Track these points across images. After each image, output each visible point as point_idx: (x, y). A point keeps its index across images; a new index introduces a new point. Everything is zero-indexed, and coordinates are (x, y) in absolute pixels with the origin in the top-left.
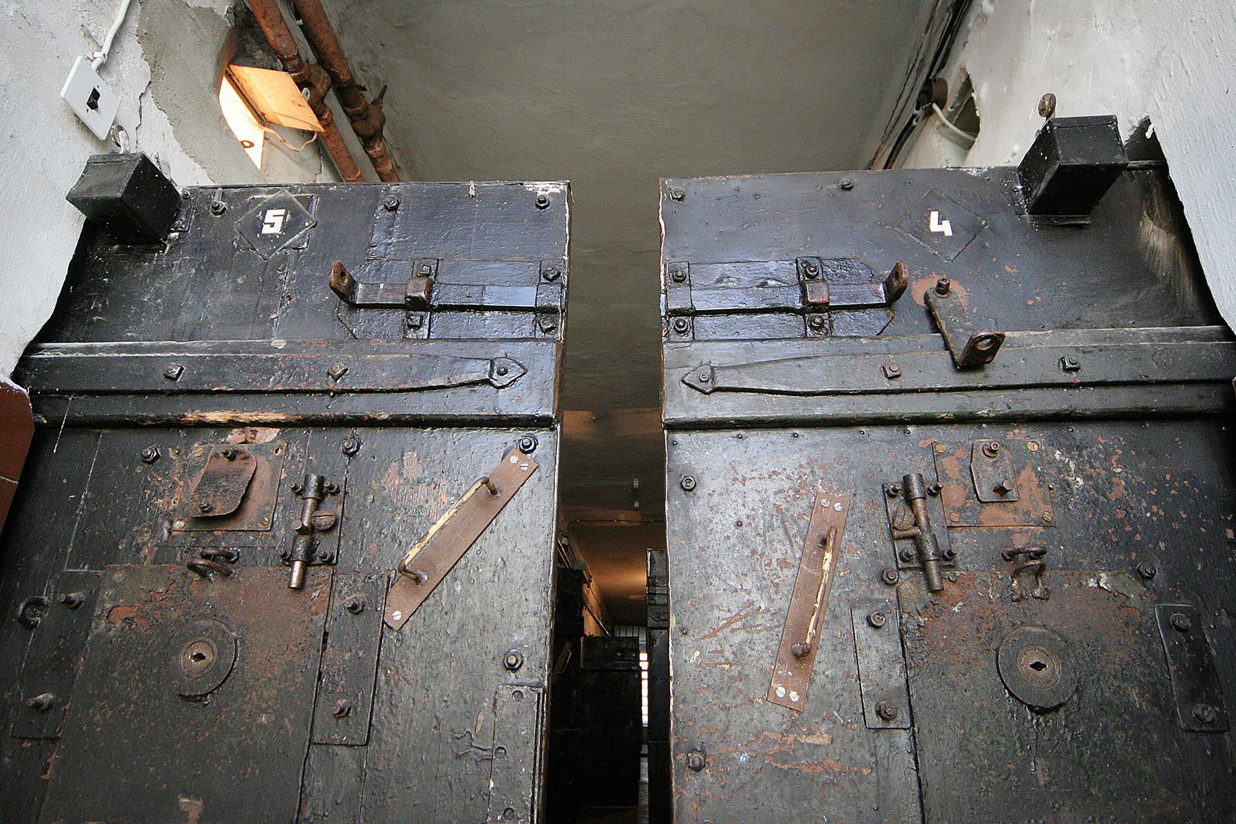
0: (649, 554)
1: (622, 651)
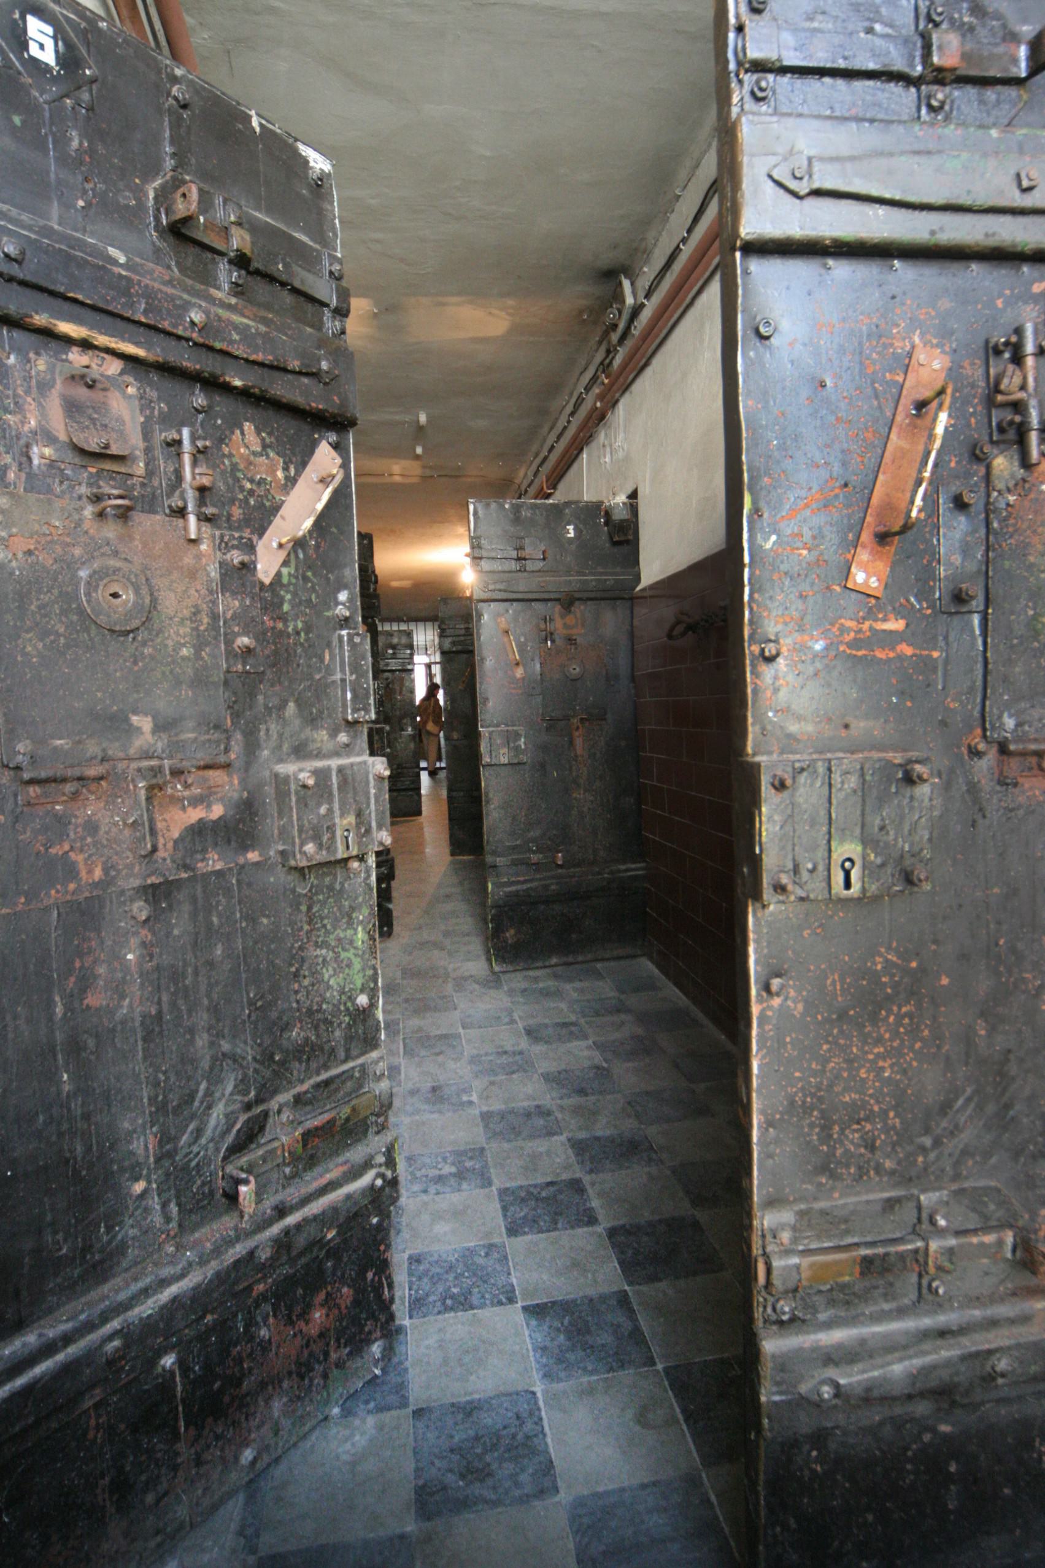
0: (471, 507)
1: (394, 647)
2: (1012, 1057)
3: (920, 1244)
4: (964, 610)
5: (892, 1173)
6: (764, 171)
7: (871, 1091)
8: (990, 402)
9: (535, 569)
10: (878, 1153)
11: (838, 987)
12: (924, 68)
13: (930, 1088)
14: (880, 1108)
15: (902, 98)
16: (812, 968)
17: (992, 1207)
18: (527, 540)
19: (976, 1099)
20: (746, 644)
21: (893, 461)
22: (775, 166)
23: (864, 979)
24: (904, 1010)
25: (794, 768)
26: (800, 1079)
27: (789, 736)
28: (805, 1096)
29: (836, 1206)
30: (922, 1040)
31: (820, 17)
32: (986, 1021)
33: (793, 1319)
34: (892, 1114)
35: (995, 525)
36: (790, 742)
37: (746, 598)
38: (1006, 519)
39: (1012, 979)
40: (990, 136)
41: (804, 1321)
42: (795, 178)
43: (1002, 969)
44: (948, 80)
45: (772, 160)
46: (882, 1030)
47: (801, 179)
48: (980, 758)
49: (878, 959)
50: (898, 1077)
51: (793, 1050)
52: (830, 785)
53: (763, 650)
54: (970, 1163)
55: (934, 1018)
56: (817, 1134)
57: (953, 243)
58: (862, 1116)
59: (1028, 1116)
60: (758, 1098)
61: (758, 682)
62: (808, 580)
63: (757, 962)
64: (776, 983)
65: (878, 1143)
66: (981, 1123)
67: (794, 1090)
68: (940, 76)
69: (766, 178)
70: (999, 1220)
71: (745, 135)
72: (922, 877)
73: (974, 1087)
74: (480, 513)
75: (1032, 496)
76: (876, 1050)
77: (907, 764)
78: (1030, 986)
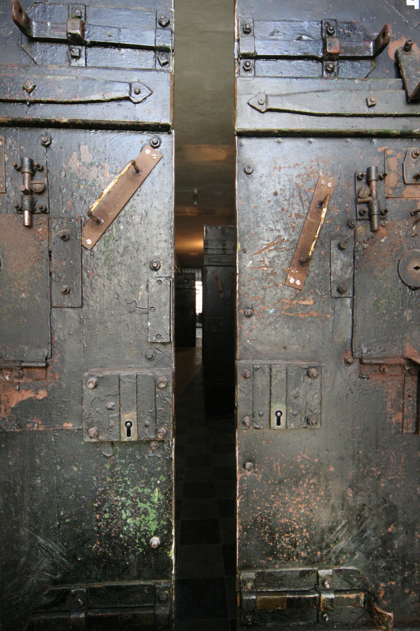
0: (205, 228)
1: (187, 279)
2: (366, 507)
3: (317, 595)
4: (344, 296)
5: (305, 558)
6: (246, 101)
7: (295, 519)
8: (357, 203)
9: (230, 253)
10: (298, 549)
11: (279, 469)
12: (323, 54)
13: (324, 519)
14: (299, 527)
15: (316, 66)
16: (266, 459)
17: (355, 580)
18: (227, 242)
19: (347, 527)
20: (237, 310)
21: (308, 228)
22: (251, 99)
23: (291, 465)
24: (311, 481)
25: (253, 368)
26: (260, 510)
27: (257, 351)
28: (262, 518)
29: (276, 572)
30: (320, 496)
31: (276, 34)
32: (353, 490)
33: (254, 625)
34: (305, 530)
35: (357, 257)
36: (258, 355)
37: (237, 289)
38: (363, 255)
39: (366, 471)
40: (355, 82)
41: (260, 626)
42: (260, 104)
43: (360, 465)
44: (335, 59)
45: (250, 96)
46: (300, 490)
47: (262, 104)
48: (350, 365)
49: (298, 457)
50: (308, 513)
51: (256, 496)
52: (271, 376)
53: (245, 312)
54: (344, 557)
55: (326, 486)
56: (268, 537)
57: (336, 131)
58: (290, 530)
59: (374, 537)
60: (239, 518)
61: (242, 326)
62: (267, 281)
63: (239, 454)
64: (248, 464)
65: (298, 544)
66: (350, 539)
67: (257, 515)
68: (332, 57)
69: (247, 105)
70: (358, 586)
71: (238, 86)
72: (313, 422)
73: (346, 521)
74: (209, 230)
75: (376, 244)
76: (297, 500)
77: (308, 368)
78: (375, 474)
